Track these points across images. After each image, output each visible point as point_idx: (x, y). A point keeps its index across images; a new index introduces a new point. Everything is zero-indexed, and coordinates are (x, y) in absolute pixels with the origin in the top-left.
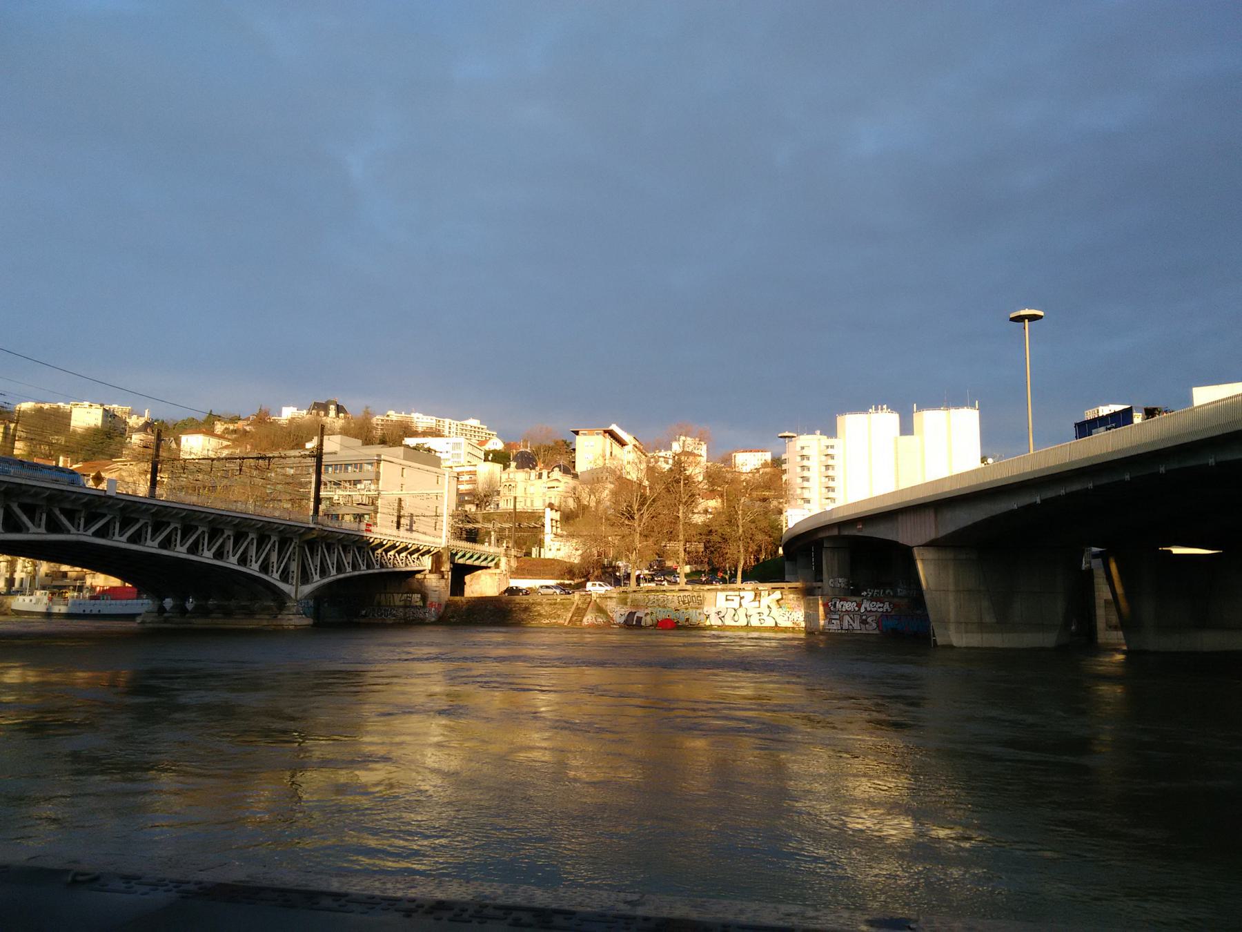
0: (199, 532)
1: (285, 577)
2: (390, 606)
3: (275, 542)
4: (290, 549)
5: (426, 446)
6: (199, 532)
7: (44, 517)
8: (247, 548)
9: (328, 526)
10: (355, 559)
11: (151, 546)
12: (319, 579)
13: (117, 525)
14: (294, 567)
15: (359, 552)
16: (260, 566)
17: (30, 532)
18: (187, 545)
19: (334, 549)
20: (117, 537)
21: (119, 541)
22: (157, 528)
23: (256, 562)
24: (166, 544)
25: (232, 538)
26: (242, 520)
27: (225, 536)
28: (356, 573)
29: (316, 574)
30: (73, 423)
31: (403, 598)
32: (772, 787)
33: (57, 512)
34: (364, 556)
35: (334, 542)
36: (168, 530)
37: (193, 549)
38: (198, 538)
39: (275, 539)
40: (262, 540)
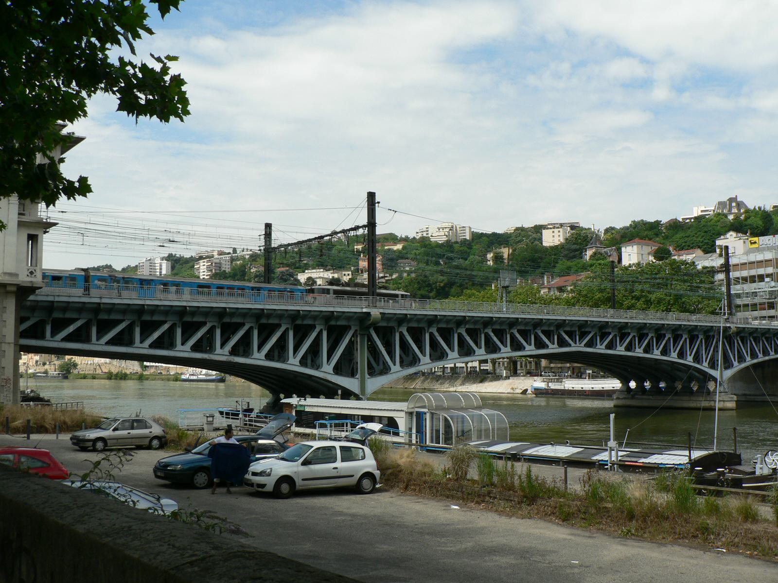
0: (649, 337)
1: (713, 365)
6: (649, 337)
7: (556, 337)
8: (698, 349)
11: (620, 350)
12: (738, 364)
15: (767, 341)
16: (709, 364)
17: (476, 354)
19: (747, 341)
20: (599, 346)
21: (601, 349)
23: (690, 355)
24: (629, 348)
28: (767, 358)
29: (735, 361)
36: (611, 337)
37: (665, 352)
38: (649, 343)
39: (635, 334)
40: (693, 339)
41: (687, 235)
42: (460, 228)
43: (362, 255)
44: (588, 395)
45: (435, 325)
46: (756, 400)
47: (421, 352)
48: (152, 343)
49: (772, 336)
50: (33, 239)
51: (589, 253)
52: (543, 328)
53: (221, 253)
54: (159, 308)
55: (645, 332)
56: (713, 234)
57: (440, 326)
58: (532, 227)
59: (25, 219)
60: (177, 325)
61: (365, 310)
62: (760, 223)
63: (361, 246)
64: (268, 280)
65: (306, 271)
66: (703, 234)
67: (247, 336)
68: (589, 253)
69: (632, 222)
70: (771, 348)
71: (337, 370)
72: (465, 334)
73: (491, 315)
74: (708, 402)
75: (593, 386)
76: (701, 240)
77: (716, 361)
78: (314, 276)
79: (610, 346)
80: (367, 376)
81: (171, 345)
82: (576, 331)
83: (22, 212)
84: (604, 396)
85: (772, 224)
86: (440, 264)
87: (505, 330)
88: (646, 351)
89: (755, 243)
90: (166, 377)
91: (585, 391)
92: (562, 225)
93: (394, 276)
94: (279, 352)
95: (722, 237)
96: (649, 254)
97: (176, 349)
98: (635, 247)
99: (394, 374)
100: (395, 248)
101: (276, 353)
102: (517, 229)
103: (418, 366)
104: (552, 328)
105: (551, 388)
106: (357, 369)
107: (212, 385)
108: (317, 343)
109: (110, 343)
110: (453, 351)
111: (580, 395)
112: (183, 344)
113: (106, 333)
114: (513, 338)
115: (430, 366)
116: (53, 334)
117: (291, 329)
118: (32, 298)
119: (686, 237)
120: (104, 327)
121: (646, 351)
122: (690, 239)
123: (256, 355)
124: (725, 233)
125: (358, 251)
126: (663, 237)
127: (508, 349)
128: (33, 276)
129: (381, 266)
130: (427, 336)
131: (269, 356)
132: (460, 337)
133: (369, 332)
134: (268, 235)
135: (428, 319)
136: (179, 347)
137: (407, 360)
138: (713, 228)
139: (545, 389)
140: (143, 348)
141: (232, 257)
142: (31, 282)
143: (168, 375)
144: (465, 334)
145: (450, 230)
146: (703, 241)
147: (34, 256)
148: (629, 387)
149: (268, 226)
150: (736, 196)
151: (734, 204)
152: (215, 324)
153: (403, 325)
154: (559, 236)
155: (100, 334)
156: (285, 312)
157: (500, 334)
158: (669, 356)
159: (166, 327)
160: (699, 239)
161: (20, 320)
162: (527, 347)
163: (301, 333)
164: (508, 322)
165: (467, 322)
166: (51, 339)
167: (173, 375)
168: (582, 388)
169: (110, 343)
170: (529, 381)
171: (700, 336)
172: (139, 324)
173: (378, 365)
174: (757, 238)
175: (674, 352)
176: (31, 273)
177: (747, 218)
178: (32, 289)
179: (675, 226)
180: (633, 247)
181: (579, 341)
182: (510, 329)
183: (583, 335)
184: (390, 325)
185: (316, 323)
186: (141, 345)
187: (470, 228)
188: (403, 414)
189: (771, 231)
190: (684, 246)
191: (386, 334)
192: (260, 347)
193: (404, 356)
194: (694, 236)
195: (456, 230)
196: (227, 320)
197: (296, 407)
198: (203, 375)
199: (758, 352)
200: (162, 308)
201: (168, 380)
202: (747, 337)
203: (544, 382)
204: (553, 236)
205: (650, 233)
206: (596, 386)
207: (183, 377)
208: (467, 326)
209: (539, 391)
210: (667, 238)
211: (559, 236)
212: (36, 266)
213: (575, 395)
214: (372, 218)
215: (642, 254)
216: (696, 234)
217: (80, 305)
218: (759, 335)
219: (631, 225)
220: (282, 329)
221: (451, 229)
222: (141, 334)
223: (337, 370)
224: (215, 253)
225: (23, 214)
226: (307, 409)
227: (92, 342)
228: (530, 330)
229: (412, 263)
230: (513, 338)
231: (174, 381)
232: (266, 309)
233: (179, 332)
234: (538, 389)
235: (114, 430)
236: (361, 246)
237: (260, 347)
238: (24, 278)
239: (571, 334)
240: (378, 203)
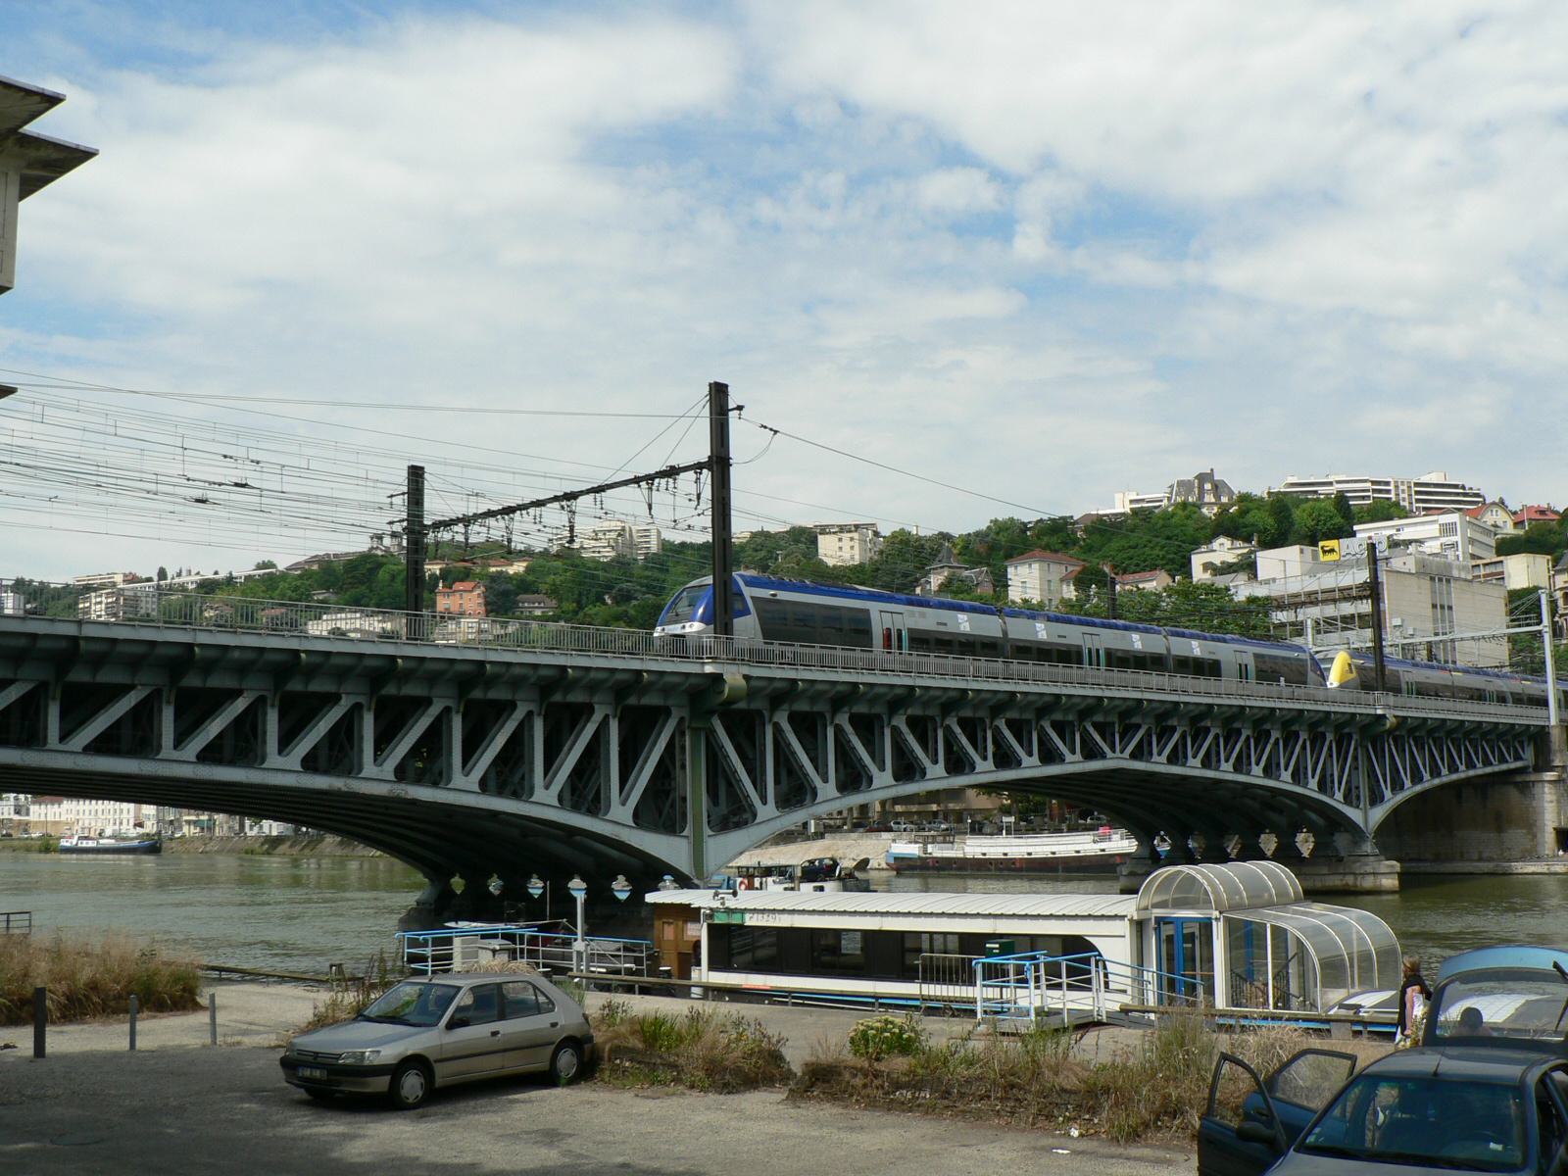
3: (1305, 741)
10: (1214, 748)
17: (928, 777)
23: (1257, 764)
25: (1252, 741)
26: (423, 987)
32: (1493, 903)
36: (1176, 736)
40: (1317, 739)
41: (1131, 543)
42: (638, 531)
43: (441, 585)
44: (1020, 870)
45: (786, 706)
46: (1412, 870)
48: (204, 750)
51: (936, 580)
53: (132, 579)
56: (1183, 542)
58: (786, 532)
60: (269, 702)
61: (709, 669)
62: (1271, 521)
63: (439, 567)
64: (416, 602)
65: (325, 617)
66: (1164, 542)
68: (936, 580)
69: (991, 521)
71: (640, 819)
73: (961, 685)
74: (1341, 877)
75: (1030, 850)
76: (1161, 553)
78: (342, 625)
80: (707, 831)
82: (1114, 723)
84: (1057, 871)
85: (1292, 524)
86: (604, 603)
87: (982, 720)
88: (1237, 769)
89: (1332, 551)
90: (22, 843)
91: (1013, 861)
93: (510, 629)
95: (1204, 548)
96: (1062, 580)
97: (264, 766)
98: (1036, 566)
99: (763, 826)
100: (511, 570)
102: (754, 535)
103: (813, 805)
104: (1070, 718)
105: (935, 855)
106: (684, 815)
107: (126, 859)
108: (593, 754)
110: (882, 768)
111: (1001, 870)
114: (999, 740)
117: (539, 715)
119: (1130, 547)
122: (1139, 551)
123: (458, 779)
124: (1209, 540)
125: (433, 576)
126: (1081, 547)
129: (484, 608)
133: (712, 724)
136: (273, 759)
138: (1182, 530)
139: (920, 858)
141: (159, 587)
143: (27, 839)
145: (619, 535)
146: (1164, 558)
148: (1153, 849)
149: (416, 474)
150: (1212, 470)
151: (1208, 486)
152: (361, 699)
154: (852, 548)
156: (504, 670)
159: (240, 705)
160: (1156, 552)
162: (1026, 761)
163: (562, 723)
164: (944, 699)
166: (61, 747)
167: (39, 838)
168: (1005, 854)
170: (869, 842)
171: (1327, 734)
172: (58, 694)
174: (1336, 541)
177: (1243, 513)
179: (1103, 528)
180: (1030, 565)
183: (1128, 731)
185: (596, 699)
186: (176, 755)
187: (659, 532)
188: (1124, 928)
189: (1291, 538)
190: (1128, 565)
194: (1145, 546)
195: (631, 535)
197: (711, 916)
198: (109, 838)
199: (1475, 760)
200: (236, 654)
201: (28, 849)
203: (916, 842)
204: (840, 548)
205: (1054, 540)
206: (1038, 849)
207: (64, 843)
208: (910, 711)
209: (904, 863)
210: (1090, 551)
211: (852, 548)
213: (989, 870)
214: (722, 445)
215: (1049, 581)
216: (1150, 542)
217: (22, 642)
219: (989, 528)
220: (597, 717)
221: (621, 533)
224: (118, 579)
226: (751, 921)
227: (48, 747)
229: (547, 600)
230: (999, 740)
231: (40, 851)
232: (490, 662)
233: (272, 720)
234: (903, 859)
235: (452, 1025)
236: (439, 567)
239: (1103, 729)
240: (740, 408)
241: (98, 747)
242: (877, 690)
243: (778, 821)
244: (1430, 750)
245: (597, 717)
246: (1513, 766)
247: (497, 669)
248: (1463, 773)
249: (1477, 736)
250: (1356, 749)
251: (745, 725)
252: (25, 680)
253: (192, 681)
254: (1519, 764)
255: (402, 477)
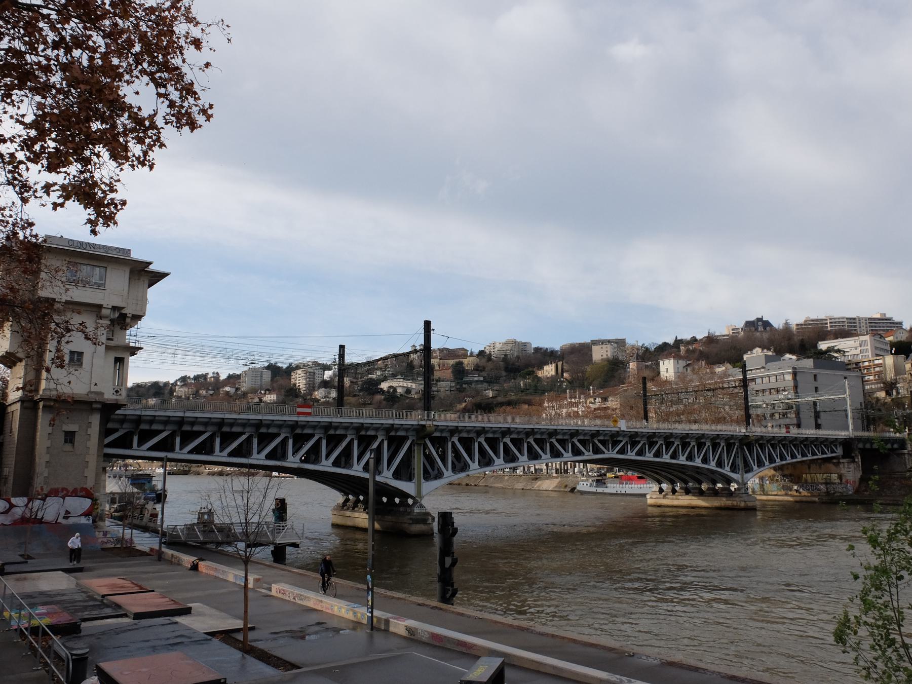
0: (675, 445)
1: (734, 469)
2: (815, 483)
3: (709, 446)
4: (735, 450)
5: (836, 348)
6: (675, 445)
7: (591, 445)
9: (758, 433)
13: (647, 446)
14: (740, 462)
15: (805, 448)
16: (730, 468)
18: (669, 454)
19: (765, 447)
20: (629, 453)
22: (634, 444)
25: (680, 447)
27: (691, 446)
30: (594, 359)
31: (824, 477)
33: (597, 442)
34: (788, 450)
35: (544, 437)
37: (674, 456)
39: (679, 443)
47: (471, 459)
49: (776, 442)
50: (120, 362)
52: (579, 438)
54: (238, 421)
55: (671, 440)
57: (512, 436)
59: (111, 343)
67: (317, 444)
70: (788, 453)
71: (397, 475)
72: (533, 443)
77: (737, 466)
79: (640, 453)
81: (248, 454)
83: (111, 337)
88: (673, 457)
92: (609, 341)
94: (344, 459)
101: (343, 459)
103: (468, 471)
109: (231, 455)
110: (499, 458)
112: (258, 453)
113: (187, 445)
114: (552, 446)
115: (479, 471)
116: (140, 444)
118: (118, 412)
120: (145, 437)
121: (673, 457)
127: (570, 454)
128: (118, 394)
130: (476, 445)
131: (336, 463)
132: (506, 446)
133: (425, 442)
134: (342, 355)
135: (592, 433)
136: (255, 455)
137: (458, 466)
140: (183, 454)
142: (116, 400)
144: (533, 443)
147: (121, 376)
149: (342, 348)
152: (288, 435)
153: (455, 435)
154: (607, 351)
155: (183, 445)
157: (562, 442)
158: (709, 465)
159: (244, 437)
161: (105, 432)
165: (460, 432)
166: (180, 452)
169: (231, 455)
172: (179, 434)
173: (433, 470)
175: (698, 458)
176: (117, 392)
178: (118, 406)
181: (612, 448)
182: (527, 438)
183: (615, 443)
184: (496, 436)
185: (315, 432)
186: (220, 454)
191: (439, 443)
192: (327, 456)
193: (456, 463)
196: (298, 431)
202: (765, 444)
212: (122, 385)
218: (764, 442)
220: (379, 440)
222: (259, 444)
223: (397, 475)
225: (112, 340)
228: (567, 440)
230: (552, 446)
237: (327, 456)
238: (109, 396)
239: (603, 443)
241: (191, 452)
242: (606, 432)
243: (360, 473)
244: (757, 449)
245: (379, 440)
246: (830, 455)
247: (462, 428)
248: (799, 458)
249: (808, 443)
250: (737, 449)
251: (439, 443)
252: (169, 430)
253: (263, 430)
254: (834, 455)
255: (337, 351)
